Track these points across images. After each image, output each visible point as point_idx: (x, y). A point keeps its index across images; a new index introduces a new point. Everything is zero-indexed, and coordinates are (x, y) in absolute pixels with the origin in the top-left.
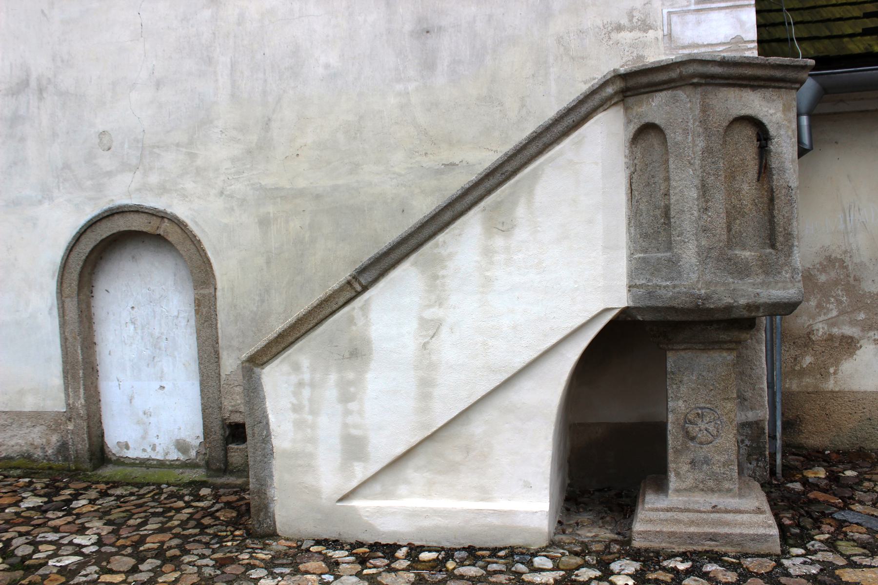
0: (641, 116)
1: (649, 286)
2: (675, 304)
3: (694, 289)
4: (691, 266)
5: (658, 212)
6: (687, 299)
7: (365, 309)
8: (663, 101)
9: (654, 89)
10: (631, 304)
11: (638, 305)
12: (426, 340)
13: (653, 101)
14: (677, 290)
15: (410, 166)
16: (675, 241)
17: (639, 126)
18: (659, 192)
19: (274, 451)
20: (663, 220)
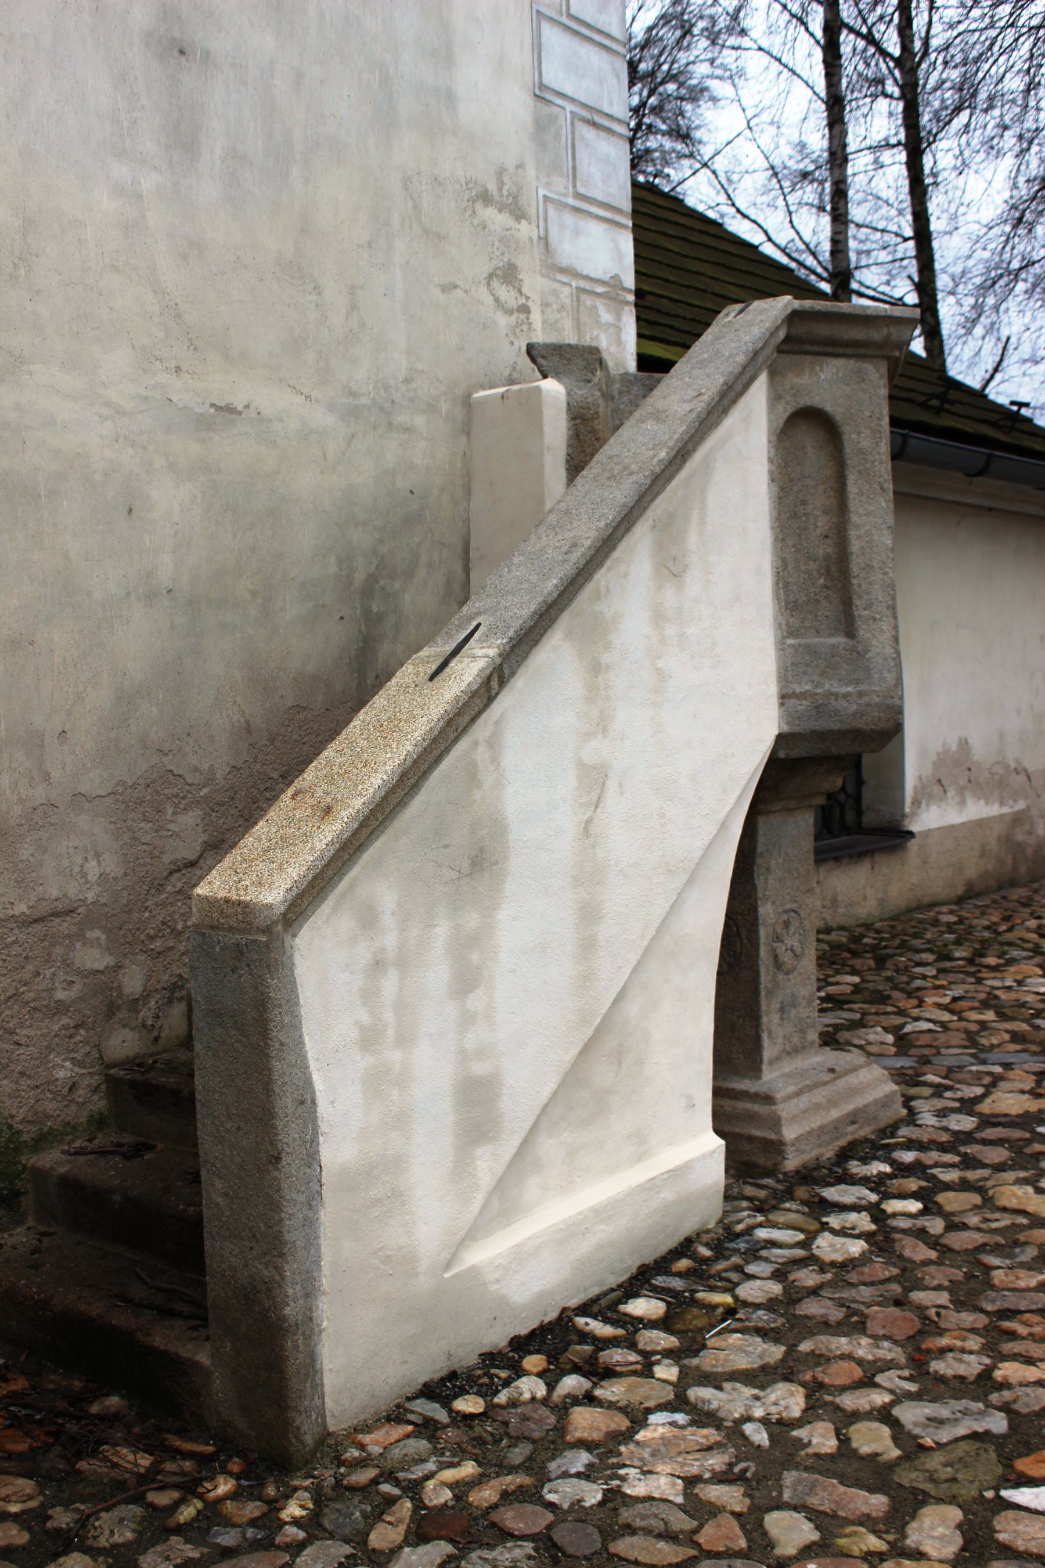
0: (798, 391)
1: (816, 694)
2: (860, 724)
3: (892, 697)
4: (885, 659)
5: (813, 566)
6: (882, 715)
7: (494, 743)
8: (840, 375)
9: (830, 350)
10: (786, 729)
11: (797, 729)
12: (589, 814)
13: (821, 370)
14: (866, 699)
15: (144, 393)
16: (860, 616)
17: (794, 409)
18: (815, 530)
19: (324, 1180)
20: (822, 581)
